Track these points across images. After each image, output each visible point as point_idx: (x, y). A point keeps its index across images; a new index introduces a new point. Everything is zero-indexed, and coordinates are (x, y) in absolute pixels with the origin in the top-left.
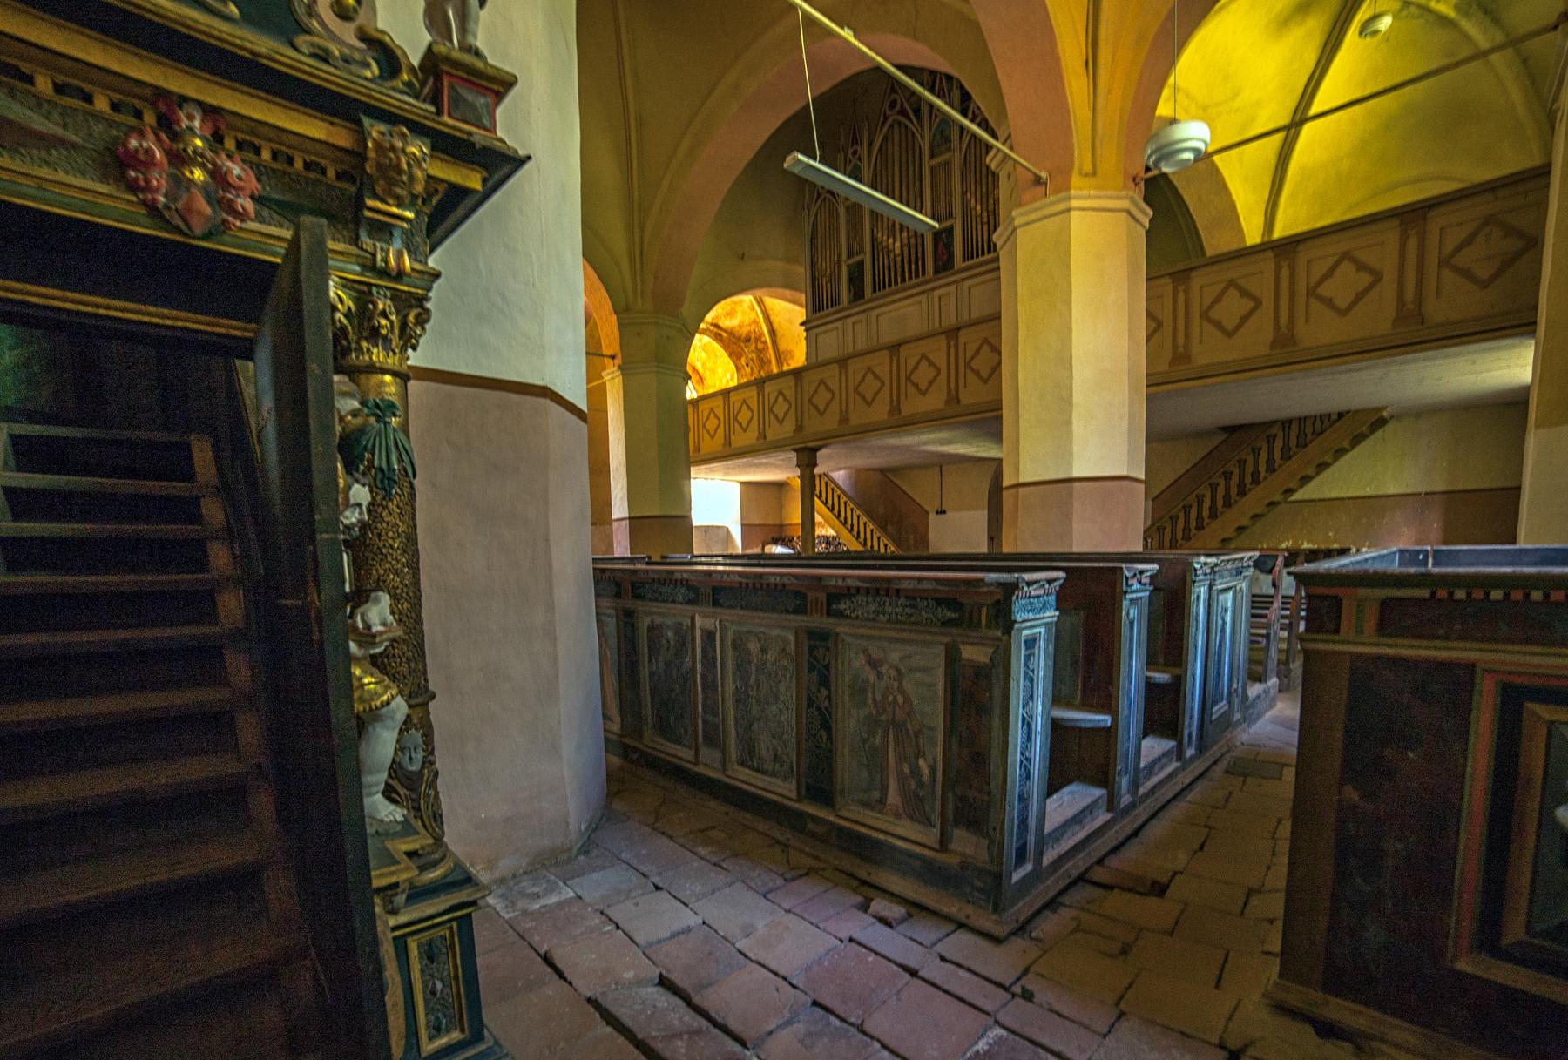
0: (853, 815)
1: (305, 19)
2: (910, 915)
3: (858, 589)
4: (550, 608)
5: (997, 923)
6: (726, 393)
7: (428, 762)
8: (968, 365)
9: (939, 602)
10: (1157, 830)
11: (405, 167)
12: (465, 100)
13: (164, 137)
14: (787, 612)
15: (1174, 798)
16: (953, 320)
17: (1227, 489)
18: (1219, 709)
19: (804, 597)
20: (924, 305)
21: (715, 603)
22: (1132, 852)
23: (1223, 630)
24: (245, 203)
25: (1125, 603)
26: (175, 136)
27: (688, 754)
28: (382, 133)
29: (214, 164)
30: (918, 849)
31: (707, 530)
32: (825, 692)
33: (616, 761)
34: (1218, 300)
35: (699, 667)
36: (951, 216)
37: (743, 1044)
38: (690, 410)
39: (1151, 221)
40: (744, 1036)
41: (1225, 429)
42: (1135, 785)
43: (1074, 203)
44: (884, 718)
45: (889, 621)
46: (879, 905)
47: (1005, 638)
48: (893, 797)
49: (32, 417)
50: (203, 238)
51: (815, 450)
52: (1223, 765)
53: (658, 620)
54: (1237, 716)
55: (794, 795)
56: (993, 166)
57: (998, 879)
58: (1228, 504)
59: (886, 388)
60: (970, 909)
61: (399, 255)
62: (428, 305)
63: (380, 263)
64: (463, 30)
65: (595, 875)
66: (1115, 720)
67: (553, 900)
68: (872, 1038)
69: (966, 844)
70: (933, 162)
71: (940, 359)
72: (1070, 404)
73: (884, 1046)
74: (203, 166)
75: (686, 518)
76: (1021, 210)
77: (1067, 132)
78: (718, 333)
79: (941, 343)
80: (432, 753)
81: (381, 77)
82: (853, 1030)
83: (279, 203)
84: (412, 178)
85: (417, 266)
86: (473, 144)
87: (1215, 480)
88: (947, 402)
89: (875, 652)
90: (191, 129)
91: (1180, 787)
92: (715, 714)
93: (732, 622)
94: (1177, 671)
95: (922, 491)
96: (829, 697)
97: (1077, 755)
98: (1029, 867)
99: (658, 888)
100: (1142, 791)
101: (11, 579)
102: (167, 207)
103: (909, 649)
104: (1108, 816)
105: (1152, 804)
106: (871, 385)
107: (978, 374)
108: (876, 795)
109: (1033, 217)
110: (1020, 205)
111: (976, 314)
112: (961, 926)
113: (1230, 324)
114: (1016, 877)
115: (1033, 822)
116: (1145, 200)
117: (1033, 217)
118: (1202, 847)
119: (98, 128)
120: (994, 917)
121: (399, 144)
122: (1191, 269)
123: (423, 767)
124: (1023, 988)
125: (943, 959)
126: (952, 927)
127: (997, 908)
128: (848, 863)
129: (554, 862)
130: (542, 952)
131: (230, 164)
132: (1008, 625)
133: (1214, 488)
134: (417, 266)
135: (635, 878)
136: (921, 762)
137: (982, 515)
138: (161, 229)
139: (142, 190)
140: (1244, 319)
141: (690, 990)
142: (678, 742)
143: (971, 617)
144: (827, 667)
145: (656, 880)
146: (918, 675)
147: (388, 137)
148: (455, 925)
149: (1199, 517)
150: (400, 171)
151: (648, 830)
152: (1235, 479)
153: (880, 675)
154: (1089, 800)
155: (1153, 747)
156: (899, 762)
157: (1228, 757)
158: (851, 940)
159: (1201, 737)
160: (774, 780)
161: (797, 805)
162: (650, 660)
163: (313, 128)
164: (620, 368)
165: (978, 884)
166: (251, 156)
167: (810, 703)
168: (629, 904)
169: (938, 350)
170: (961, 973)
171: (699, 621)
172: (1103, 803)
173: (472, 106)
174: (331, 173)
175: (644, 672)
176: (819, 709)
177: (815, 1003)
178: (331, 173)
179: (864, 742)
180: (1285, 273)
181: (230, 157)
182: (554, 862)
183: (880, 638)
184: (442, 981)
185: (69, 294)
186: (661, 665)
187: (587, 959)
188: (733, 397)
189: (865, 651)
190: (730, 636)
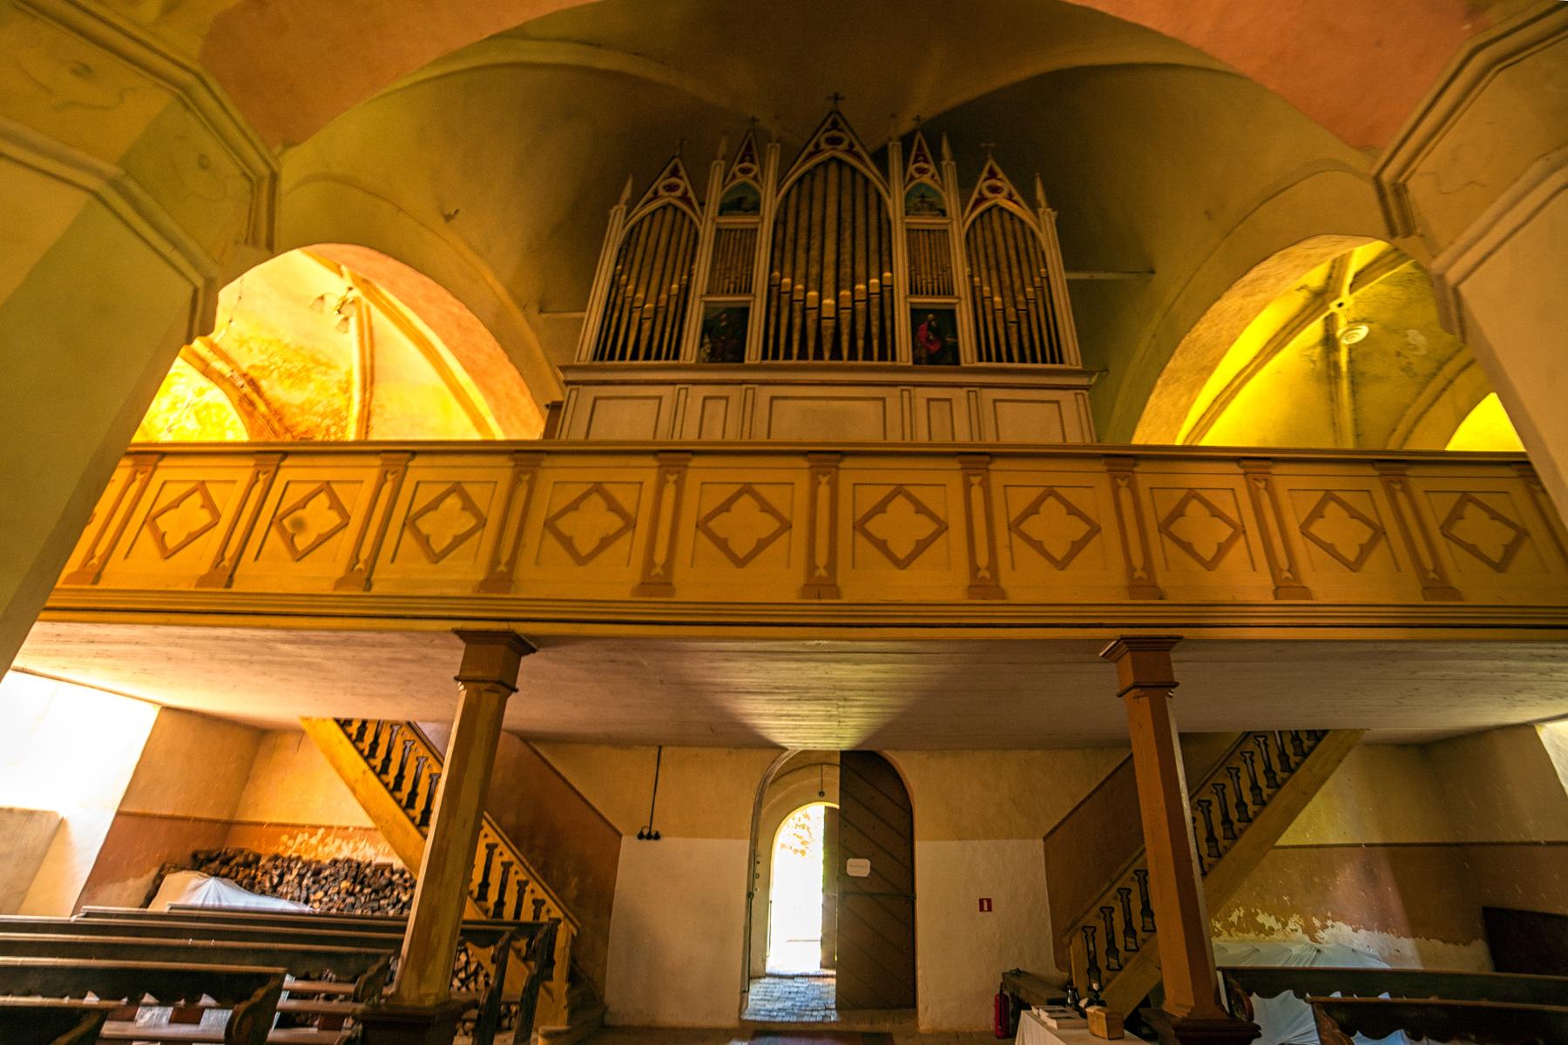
38: (121, 474)
51: (523, 646)
56: (1452, 276)
59: (347, 538)
71: (357, 499)
101: (886, 1027)
106: (319, 516)
113: (742, 548)
140: (605, 543)
180: (824, 491)
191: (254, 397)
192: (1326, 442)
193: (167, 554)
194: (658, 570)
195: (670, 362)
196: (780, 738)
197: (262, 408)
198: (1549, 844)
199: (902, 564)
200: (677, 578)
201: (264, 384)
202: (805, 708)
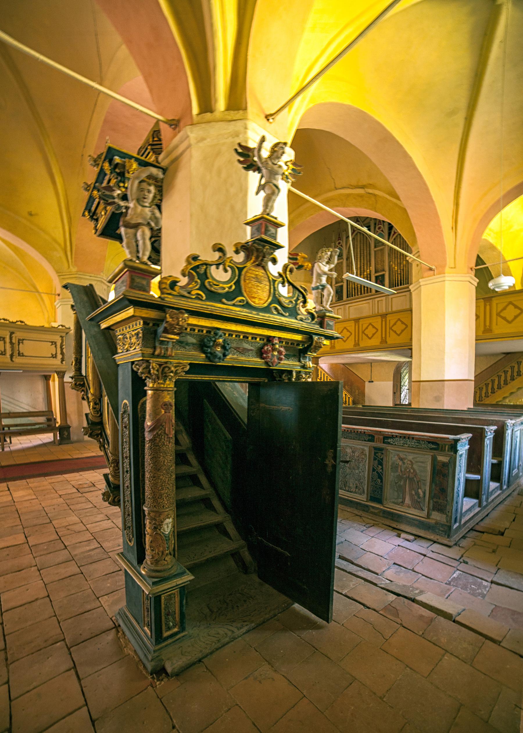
0: (390, 506)
2: (415, 539)
3: (396, 436)
5: (449, 541)
8: (391, 328)
9: (429, 442)
10: (495, 514)
14: (365, 441)
15: (500, 503)
16: (384, 311)
17: (506, 377)
18: (515, 471)
19: (374, 437)
20: (371, 303)
22: (487, 521)
23: (516, 444)
25: (486, 440)
30: (418, 518)
32: (380, 467)
34: (504, 309)
36: (383, 270)
37: (377, 574)
39: (478, 283)
40: (377, 572)
41: (504, 353)
42: (487, 499)
43: (447, 278)
44: (405, 476)
45: (409, 447)
46: (403, 535)
47: (454, 455)
48: (408, 501)
52: (516, 493)
54: (521, 474)
55: (365, 500)
57: (450, 527)
58: (506, 383)
60: (438, 537)
66: (482, 478)
68: (418, 573)
69: (436, 516)
70: (376, 249)
72: (444, 352)
73: (423, 575)
76: (424, 279)
77: (444, 252)
79: (379, 319)
82: (411, 571)
87: (500, 374)
88: (381, 343)
89: (402, 455)
91: (502, 500)
94: (500, 459)
95: (363, 373)
96: (382, 469)
97: (473, 490)
98: (457, 524)
100: (490, 500)
103: (416, 456)
104: (479, 509)
105: (492, 505)
107: (395, 332)
108: (401, 500)
109: (428, 282)
110: (423, 278)
111: (394, 309)
112: (435, 542)
114: (454, 527)
115: (459, 510)
116: (475, 276)
117: (428, 282)
118: (514, 520)
120: (448, 539)
122: (492, 297)
124: (463, 560)
125: (433, 552)
126: (432, 543)
127: (449, 536)
128: (388, 522)
132: (456, 451)
133: (499, 377)
136: (420, 490)
137: (391, 384)
143: (442, 447)
144: (382, 459)
146: (420, 464)
149: (493, 388)
152: (509, 374)
153: (404, 463)
154: (472, 504)
155: (493, 485)
156: (410, 490)
157: (518, 489)
158: (399, 546)
159: (508, 482)
160: (355, 494)
161: (366, 503)
163: (298, 337)
165: (441, 529)
167: (374, 470)
169: (377, 322)
170: (440, 556)
172: (477, 504)
176: (377, 472)
177: (394, 564)
179: (396, 483)
183: (404, 452)
189: (398, 455)
192: (371, 314)
194: (488, 327)
195: (369, 294)
199: (370, 338)
200: (336, 346)
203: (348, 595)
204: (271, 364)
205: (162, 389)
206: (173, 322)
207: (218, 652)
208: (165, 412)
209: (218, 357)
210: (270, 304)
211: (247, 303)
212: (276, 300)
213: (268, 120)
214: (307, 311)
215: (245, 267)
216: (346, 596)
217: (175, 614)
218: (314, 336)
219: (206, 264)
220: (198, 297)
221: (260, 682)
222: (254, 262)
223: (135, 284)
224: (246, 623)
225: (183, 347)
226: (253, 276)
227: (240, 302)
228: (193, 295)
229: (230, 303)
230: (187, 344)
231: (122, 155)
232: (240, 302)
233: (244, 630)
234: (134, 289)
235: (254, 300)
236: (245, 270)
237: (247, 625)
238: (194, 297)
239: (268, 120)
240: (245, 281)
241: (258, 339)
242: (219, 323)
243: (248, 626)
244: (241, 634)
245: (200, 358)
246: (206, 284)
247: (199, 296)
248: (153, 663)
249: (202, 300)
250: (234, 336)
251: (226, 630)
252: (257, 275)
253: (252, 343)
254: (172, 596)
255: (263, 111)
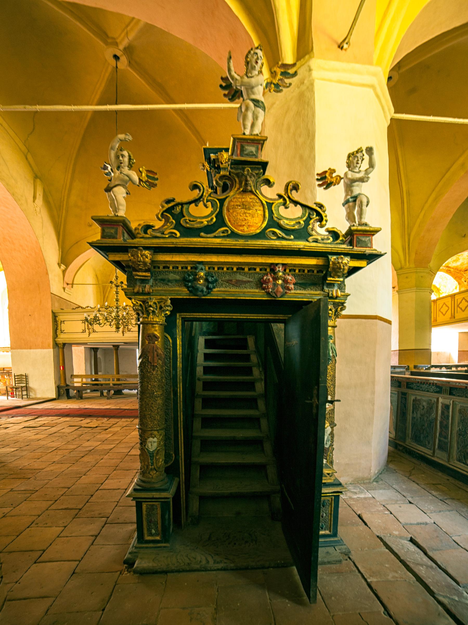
1: (311, 232)
4: (373, 393)
6: (453, 296)
7: (331, 445)
11: (342, 267)
12: (361, 240)
13: (272, 274)
21: (451, 394)
24: (292, 286)
26: (275, 273)
27: (430, 452)
28: (335, 259)
29: (284, 278)
31: (438, 354)
33: (392, 449)
35: (439, 418)
49: (209, 334)
50: (280, 297)
53: (418, 398)
61: (337, 291)
62: (345, 305)
63: (330, 295)
64: (361, 218)
65: (381, 491)
67: (362, 496)
74: (281, 279)
75: (430, 350)
78: (449, 271)
80: (333, 443)
81: (333, 241)
83: (300, 284)
84: (344, 269)
85: (343, 294)
86: (366, 254)
90: (279, 271)
92: (446, 438)
93: (460, 402)
99: (410, 503)
102: (272, 292)
119: (256, 276)
121: (340, 261)
123: (330, 447)
129: (363, 482)
130: (358, 513)
131: (288, 277)
134: (343, 294)
135: (399, 496)
138: (269, 297)
139: (266, 289)
141: (426, 548)
142: (425, 446)
145: (410, 499)
147: (337, 260)
148: (333, 497)
150: (340, 268)
151: (406, 479)
162: (413, 412)
163: (312, 261)
164: (397, 291)
166: (293, 273)
168: (397, 506)
171: (441, 400)
173: (365, 242)
174: (315, 272)
175: (410, 417)
178: (315, 272)
181: (289, 275)
182: (363, 482)
184: (326, 513)
185: (242, 315)
186: (419, 416)
187: (377, 521)
188: (456, 297)
190: (458, 408)
191: (449, 269)
193: (444, 315)
196: (124, 293)
197: (452, 270)
198: (418, 524)
201: (450, 265)
202: (263, 388)
203: (373, 586)
204: (274, 295)
205: (151, 322)
206: (134, 260)
207: (185, 573)
208: (149, 343)
209: (200, 290)
210: (266, 228)
211: (233, 232)
212: (273, 223)
213: (342, 48)
214: (328, 231)
215: (227, 197)
216: (369, 585)
217: (158, 524)
218: (330, 257)
219: (182, 204)
220: (172, 235)
221: (191, 620)
222: (239, 189)
223: (105, 234)
224: (225, 561)
225: (167, 284)
226: (238, 204)
227: (223, 232)
228: (166, 235)
229: (209, 235)
230: (169, 281)
231: (215, 151)
232: (223, 232)
233: (220, 566)
234: (105, 238)
235: (241, 228)
236: (227, 200)
237: (225, 563)
238: (167, 236)
239: (342, 48)
240: (228, 210)
241: (258, 270)
242: (195, 256)
243: (225, 565)
244: (215, 568)
245: (183, 293)
246: (182, 222)
247: (174, 235)
248: (130, 556)
249: (176, 238)
250: (225, 269)
251: (204, 558)
252: (243, 202)
253: (250, 274)
254: (155, 507)
255: (336, 42)
